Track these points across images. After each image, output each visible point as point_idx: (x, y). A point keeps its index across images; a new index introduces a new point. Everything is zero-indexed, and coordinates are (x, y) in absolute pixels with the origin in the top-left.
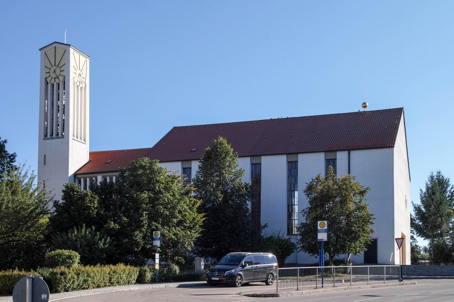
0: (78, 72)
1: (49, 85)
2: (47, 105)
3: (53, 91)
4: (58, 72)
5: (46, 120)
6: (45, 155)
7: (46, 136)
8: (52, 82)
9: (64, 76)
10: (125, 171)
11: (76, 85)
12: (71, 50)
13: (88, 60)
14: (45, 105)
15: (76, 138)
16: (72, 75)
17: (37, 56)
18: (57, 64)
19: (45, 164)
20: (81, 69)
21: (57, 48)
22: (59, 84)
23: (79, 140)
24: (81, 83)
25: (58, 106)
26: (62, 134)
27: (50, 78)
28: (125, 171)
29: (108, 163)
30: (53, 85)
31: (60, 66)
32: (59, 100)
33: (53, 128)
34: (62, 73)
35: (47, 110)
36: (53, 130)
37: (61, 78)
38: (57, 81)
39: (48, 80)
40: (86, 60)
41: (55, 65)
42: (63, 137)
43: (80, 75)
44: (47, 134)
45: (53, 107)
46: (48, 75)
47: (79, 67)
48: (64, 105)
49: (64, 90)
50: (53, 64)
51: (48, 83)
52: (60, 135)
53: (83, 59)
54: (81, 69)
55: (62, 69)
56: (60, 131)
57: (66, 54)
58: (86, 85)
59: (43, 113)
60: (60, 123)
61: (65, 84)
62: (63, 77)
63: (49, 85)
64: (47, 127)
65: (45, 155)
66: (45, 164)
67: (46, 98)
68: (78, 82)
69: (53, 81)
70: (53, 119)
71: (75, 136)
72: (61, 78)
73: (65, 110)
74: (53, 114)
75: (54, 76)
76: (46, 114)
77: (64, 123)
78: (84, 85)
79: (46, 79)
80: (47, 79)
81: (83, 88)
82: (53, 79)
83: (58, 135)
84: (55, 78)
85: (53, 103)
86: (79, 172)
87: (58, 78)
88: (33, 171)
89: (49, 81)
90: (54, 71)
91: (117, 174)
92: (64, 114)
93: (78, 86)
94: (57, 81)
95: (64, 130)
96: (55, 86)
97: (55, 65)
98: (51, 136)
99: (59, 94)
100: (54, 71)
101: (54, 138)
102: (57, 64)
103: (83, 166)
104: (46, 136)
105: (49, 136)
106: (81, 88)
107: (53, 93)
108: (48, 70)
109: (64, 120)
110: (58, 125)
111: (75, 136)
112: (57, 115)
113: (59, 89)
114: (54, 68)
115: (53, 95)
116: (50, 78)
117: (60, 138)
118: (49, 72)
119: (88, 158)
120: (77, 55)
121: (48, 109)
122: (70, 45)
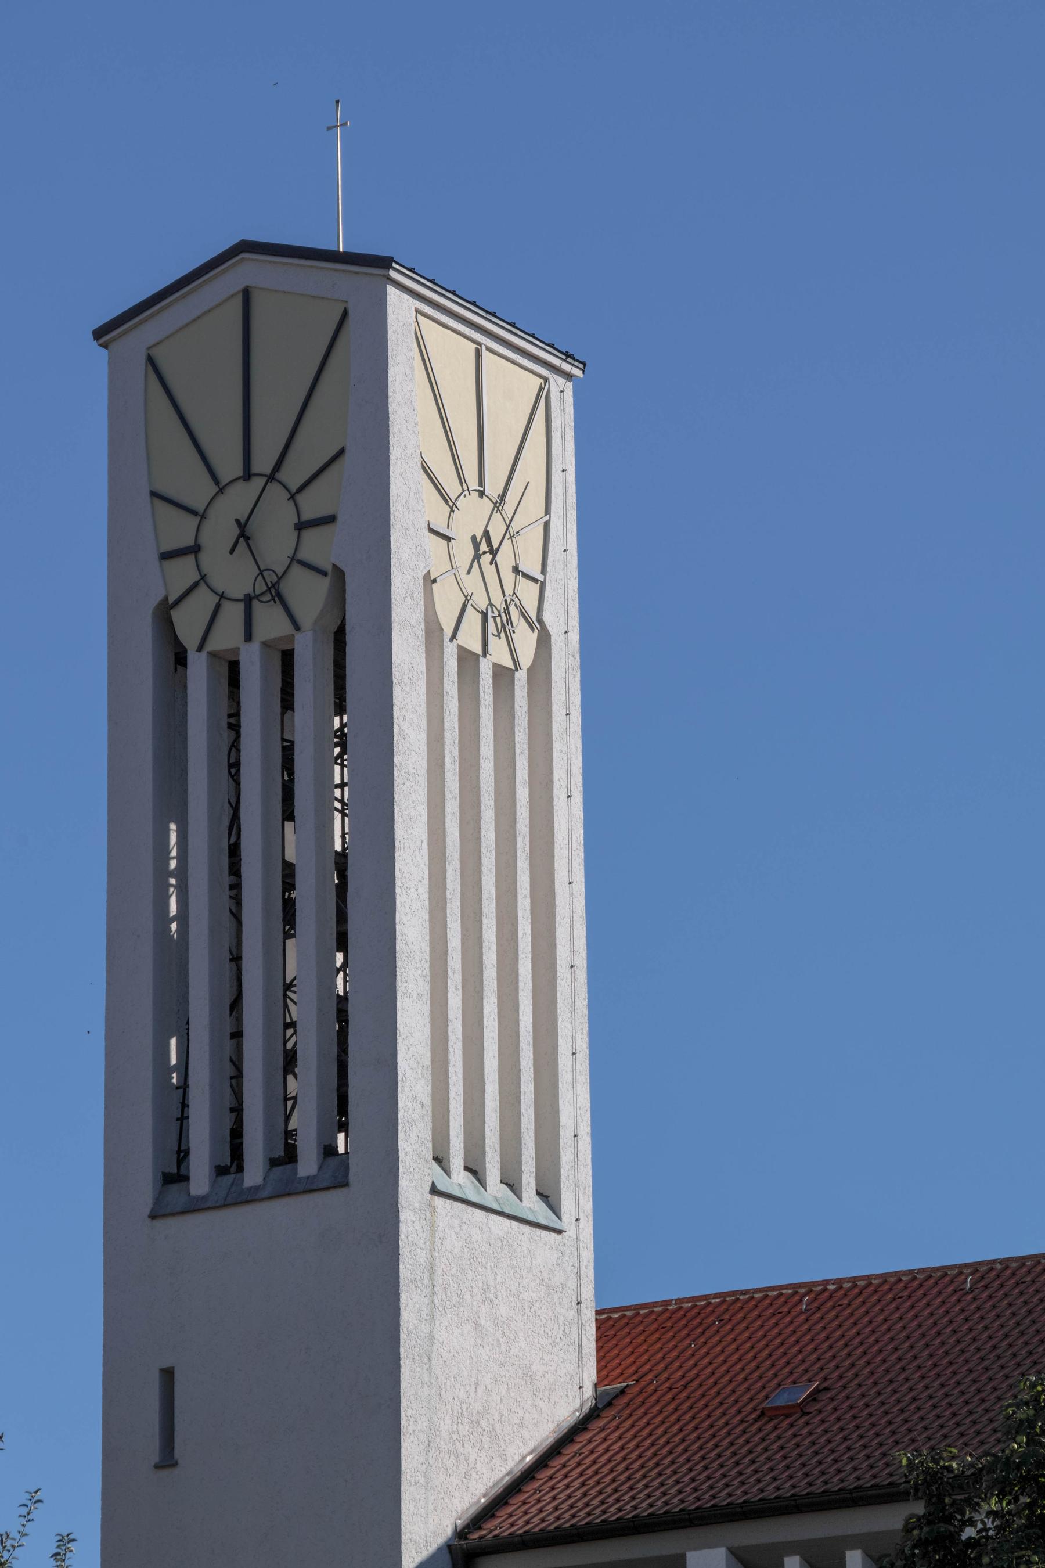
0: (472, 516)
1: (198, 671)
2: (182, 873)
3: (235, 727)
4: (276, 541)
5: (173, 1017)
6: (168, 1375)
7: (174, 1176)
8: (219, 642)
9: (339, 575)
10: (969, 1486)
11: (450, 652)
12: (400, 308)
13: (563, 396)
14: (162, 873)
15: (460, 1180)
16: (411, 554)
17: (87, 383)
18: (263, 463)
19: (167, 1460)
20: (493, 488)
21: (166, 547)
22: (288, 658)
23: (495, 1190)
24: (506, 630)
25: (289, 871)
26: (330, 1150)
27: (202, 602)
28: (969, 1486)
29: (786, 1412)
30: (234, 668)
31: (294, 474)
32: (289, 815)
33: (237, 1093)
34: (317, 546)
35: (183, 917)
36: (237, 1110)
37: (308, 595)
38: (270, 623)
39: (188, 624)
40: (542, 395)
41: (248, 475)
42: (336, 1173)
43: (485, 547)
44: (183, 1155)
45: (236, 887)
46: (183, 572)
47: (475, 457)
48: (341, 859)
49: (340, 709)
50: (229, 466)
51: (181, 659)
52: (308, 1164)
53: (512, 384)
54: (493, 488)
55: (312, 505)
56: (305, 1121)
57: (347, 361)
58: (544, 640)
59: (146, 949)
60: (311, 1044)
61: (345, 655)
62: (322, 586)
63: (198, 667)
64: (184, 1086)
65: (168, 1375)
66: (167, 1460)
67: (171, 802)
68: (473, 620)
69: (227, 635)
70: (236, 1004)
71: (457, 1162)
72: (308, 595)
73: (351, 902)
74: (236, 959)
75: (235, 576)
76: (172, 959)
77: (343, 1036)
78: (526, 641)
79: (164, 613)
80: (176, 615)
81: (521, 676)
82: (233, 613)
83: (290, 1155)
84: (248, 600)
85: (234, 851)
86: (498, 1527)
87: (279, 598)
88: (65, 1541)
89: (189, 637)
90: (244, 533)
91: (890, 1520)
92: (342, 944)
93: (468, 660)
94: (270, 623)
95: (343, 1106)
96: (251, 667)
97: (248, 475)
98: (221, 1171)
99: (288, 751)
100: (244, 533)
101: (250, 1197)
102: (263, 463)
103: (543, 1461)
104: (174, 1176)
105: (200, 1181)
106: (503, 676)
107: (235, 745)
108: (180, 530)
109: (342, 1007)
110: (290, 1061)
111: (457, 1162)
112: (276, 959)
113: (287, 703)
114: (238, 500)
115: (234, 767)
116: (202, 602)
117: (310, 1187)
118: (195, 550)
119: (590, 1374)
120: (451, 349)
121: (189, 907)
122: (384, 263)
